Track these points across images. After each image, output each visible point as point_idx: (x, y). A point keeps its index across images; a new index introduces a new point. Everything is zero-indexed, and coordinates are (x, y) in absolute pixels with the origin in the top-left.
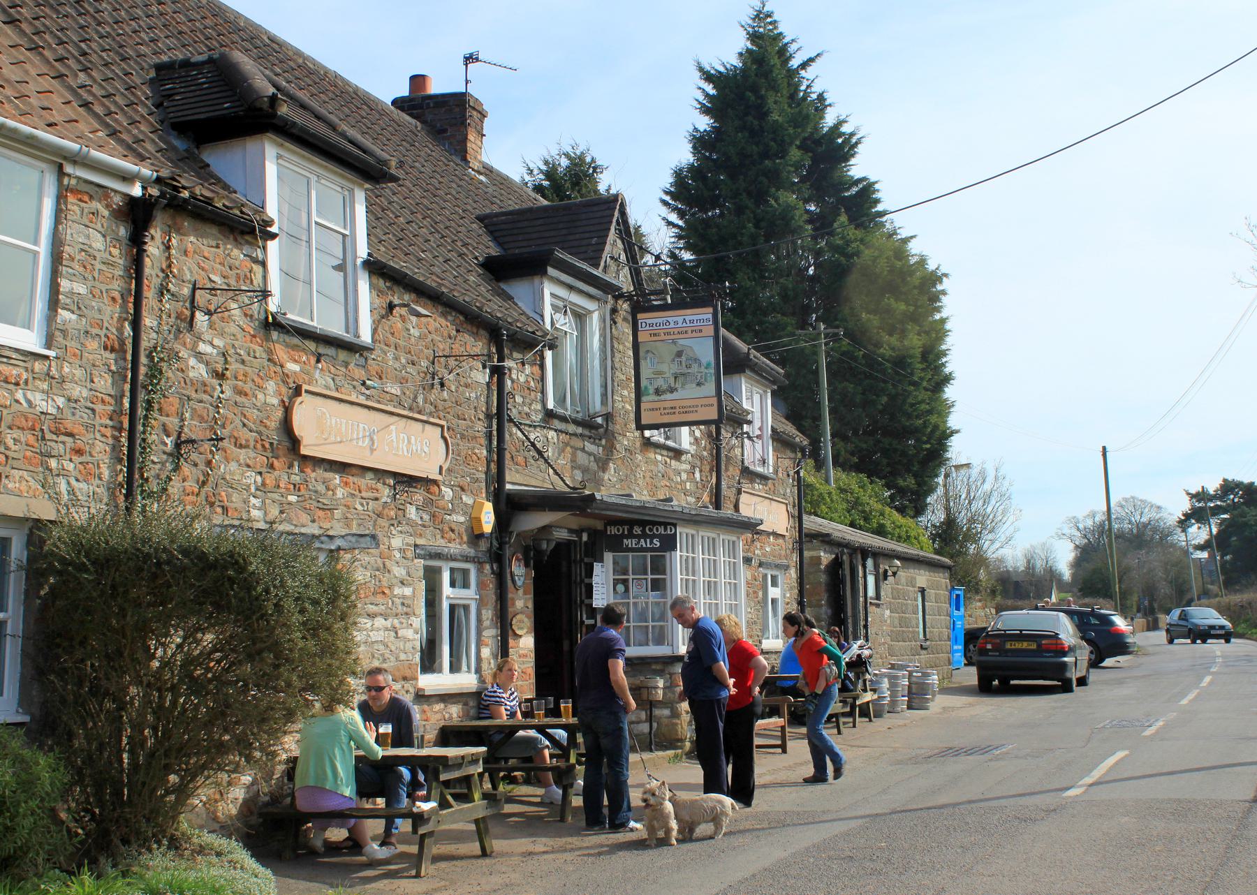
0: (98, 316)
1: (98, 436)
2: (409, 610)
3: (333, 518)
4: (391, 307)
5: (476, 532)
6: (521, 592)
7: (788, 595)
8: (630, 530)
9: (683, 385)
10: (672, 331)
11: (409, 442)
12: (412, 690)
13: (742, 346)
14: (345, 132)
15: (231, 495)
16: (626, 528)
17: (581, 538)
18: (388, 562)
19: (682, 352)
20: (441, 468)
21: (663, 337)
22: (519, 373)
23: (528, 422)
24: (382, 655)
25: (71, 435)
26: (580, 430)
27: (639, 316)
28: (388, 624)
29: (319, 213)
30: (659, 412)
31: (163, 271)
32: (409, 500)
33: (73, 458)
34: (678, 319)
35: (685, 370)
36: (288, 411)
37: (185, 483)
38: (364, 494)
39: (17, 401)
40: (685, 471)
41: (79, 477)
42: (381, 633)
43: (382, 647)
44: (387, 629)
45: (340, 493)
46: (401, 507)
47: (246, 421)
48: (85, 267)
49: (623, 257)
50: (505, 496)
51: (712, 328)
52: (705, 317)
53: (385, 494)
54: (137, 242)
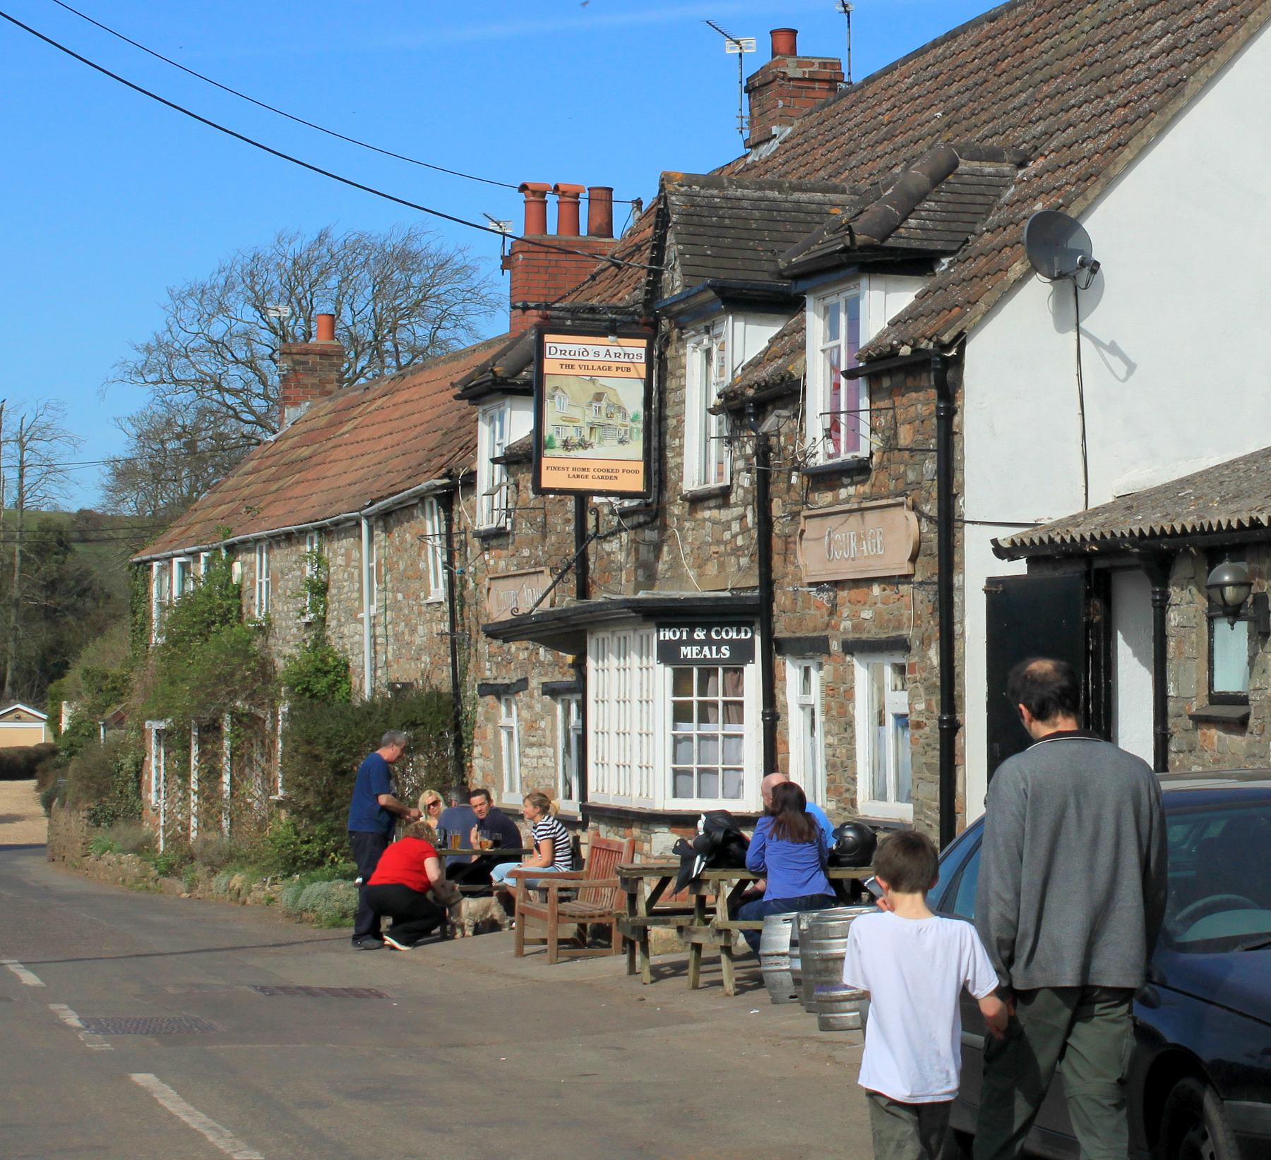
9: (601, 439)
10: (591, 364)
21: (577, 371)
30: (565, 473)
35: (603, 420)
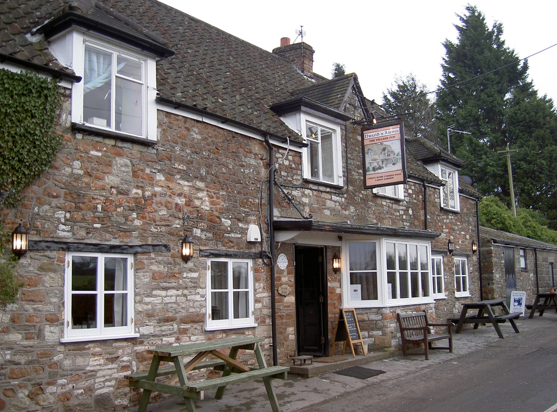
2: (195, 285)
3: (131, 236)
7: (471, 269)
9: (386, 165)
10: (380, 138)
13: (449, 149)
19: (385, 148)
21: (376, 142)
23: (290, 185)
24: (175, 310)
26: (328, 190)
27: (364, 132)
28: (180, 292)
30: (375, 179)
32: (195, 226)
34: (382, 132)
35: (387, 157)
38: (158, 223)
40: (402, 210)
43: (175, 306)
47: (57, 183)
52: (396, 129)
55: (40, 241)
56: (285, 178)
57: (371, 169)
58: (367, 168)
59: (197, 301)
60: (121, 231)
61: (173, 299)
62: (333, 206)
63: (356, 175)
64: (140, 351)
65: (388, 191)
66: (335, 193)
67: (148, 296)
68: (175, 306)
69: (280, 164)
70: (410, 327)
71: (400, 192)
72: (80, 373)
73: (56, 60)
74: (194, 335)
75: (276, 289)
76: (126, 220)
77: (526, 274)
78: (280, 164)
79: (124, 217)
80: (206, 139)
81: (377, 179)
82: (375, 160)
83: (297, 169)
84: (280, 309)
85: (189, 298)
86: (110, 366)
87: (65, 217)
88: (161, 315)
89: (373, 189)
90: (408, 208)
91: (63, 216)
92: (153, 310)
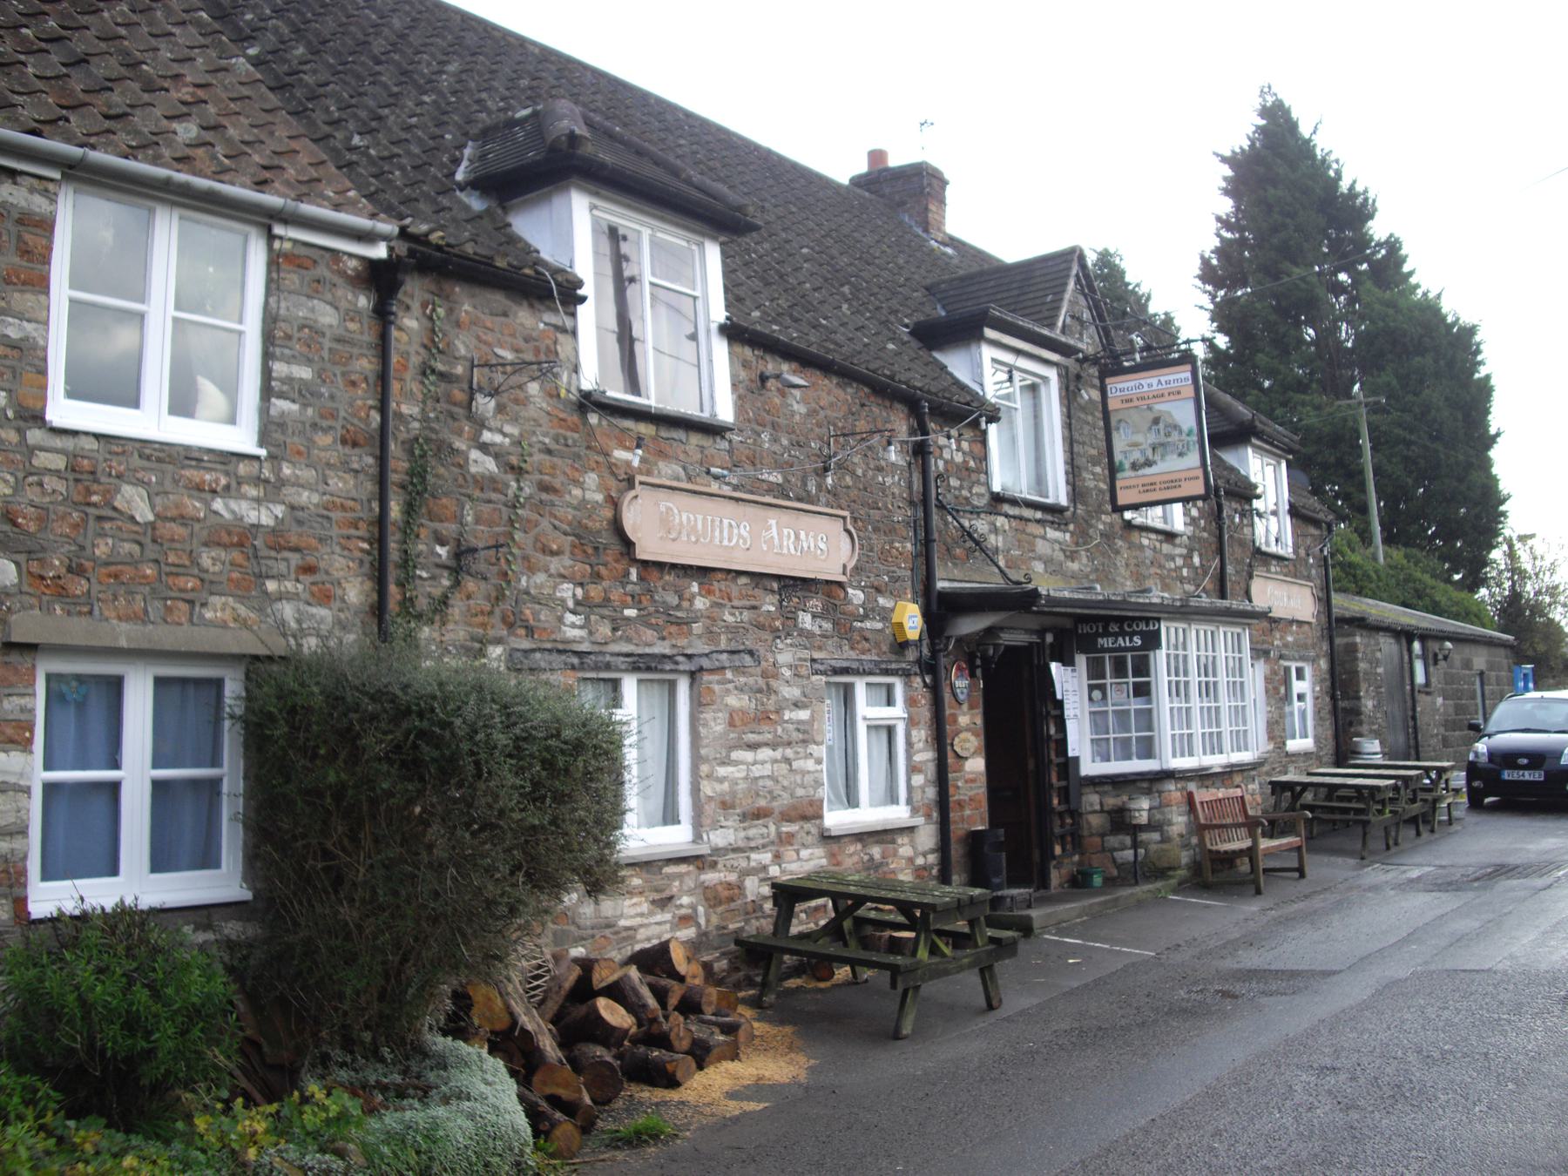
0: (330, 404)
1: (338, 549)
2: (806, 736)
3: (690, 633)
4: (763, 379)
5: (899, 640)
6: (965, 707)
8: (1105, 628)
9: (1163, 456)
11: (797, 537)
12: (814, 831)
14: (690, 177)
15: (539, 613)
16: (1100, 625)
17: (1044, 640)
18: (773, 683)
20: (845, 567)
21: (1136, 403)
22: (949, 448)
23: (968, 508)
24: (770, 792)
25: (296, 549)
26: (1039, 515)
27: (1108, 380)
28: (778, 754)
29: (653, 274)
30: (1136, 490)
31: (425, 347)
33: (301, 578)
35: (1163, 439)
36: (615, 504)
37: (472, 602)
38: (736, 603)
39: (216, 513)
40: (1180, 556)
41: (311, 601)
42: (768, 766)
43: (769, 783)
44: (775, 761)
45: (700, 603)
46: (790, 615)
47: (557, 523)
48: (309, 347)
49: (1086, 315)
50: (935, 594)
51: (1192, 387)
52: (1183, 376)
53: (769, 605)
54: (383, 315)
55: (533, 650)
56: (957, 493)
57: (1127, 465)
58: (1117, 463)
59: (809, 772)
60: (672, 623)
61: (766, 770)
62: (1049, 552)
63: (1094, 478)
64: (712, 884)
65: (1153, 517)
66: (1053, 523)
67: (723, 764)
68: (769, 783)
69: (946, 462)
70: (1214, 822)
71: (1177, 517)
72: (607, 932)
73: (538, 252)
74: (804, 846)
75: (949, 741)
76: (681, 598)
77: (1428, 698)
78: (946, 462)
79: (676, 592)
80: (815, 411)
81: (1141, 489)
82: (1135, 445)
83: (978, 471)
84: (958, 787)
85: (795, 765)
86: (659, 917)
87: (574, 595)
88: (747, 804)
89: (274, 375)
90: (1191, 550)
91: (570, 594)
92: (733, 793)
